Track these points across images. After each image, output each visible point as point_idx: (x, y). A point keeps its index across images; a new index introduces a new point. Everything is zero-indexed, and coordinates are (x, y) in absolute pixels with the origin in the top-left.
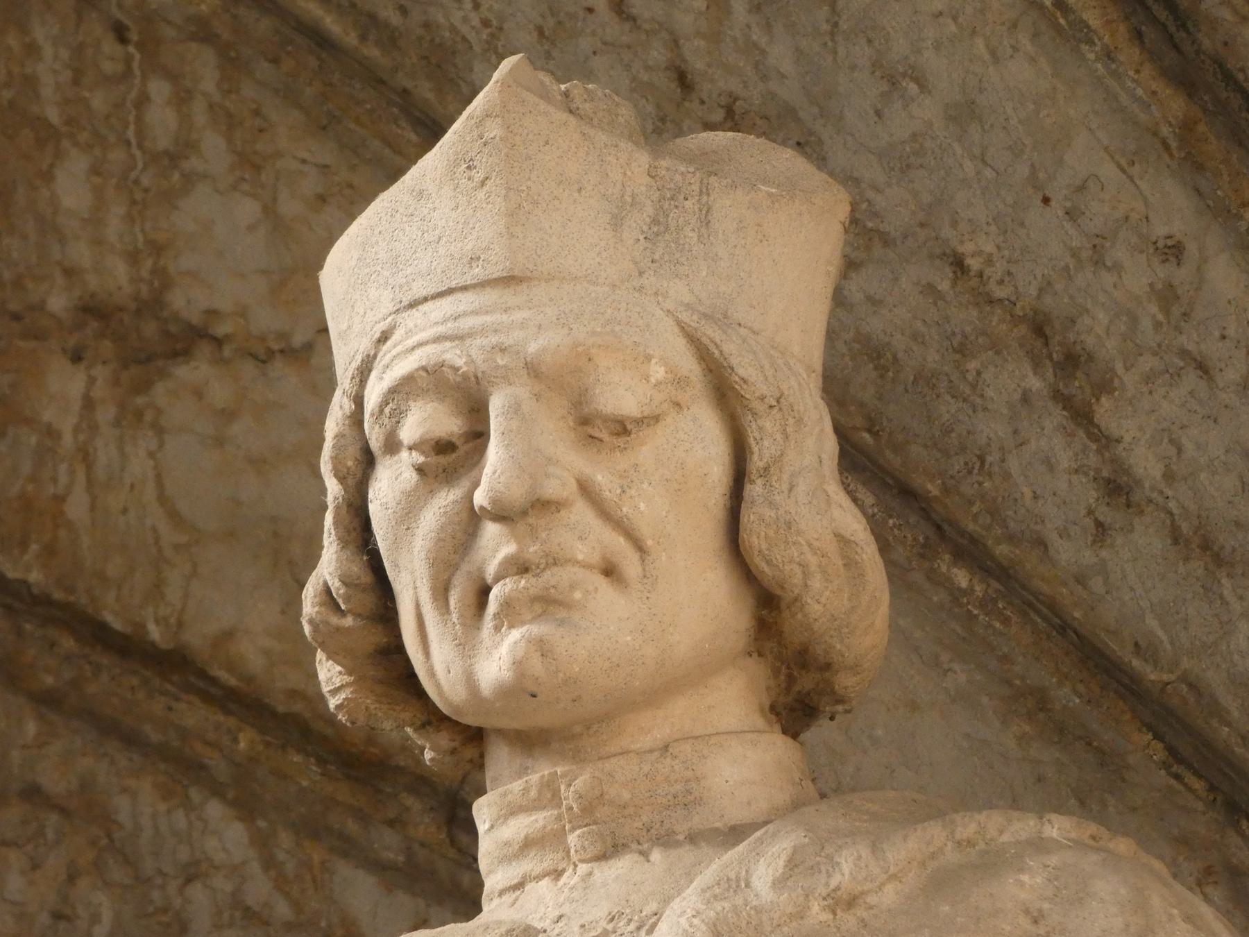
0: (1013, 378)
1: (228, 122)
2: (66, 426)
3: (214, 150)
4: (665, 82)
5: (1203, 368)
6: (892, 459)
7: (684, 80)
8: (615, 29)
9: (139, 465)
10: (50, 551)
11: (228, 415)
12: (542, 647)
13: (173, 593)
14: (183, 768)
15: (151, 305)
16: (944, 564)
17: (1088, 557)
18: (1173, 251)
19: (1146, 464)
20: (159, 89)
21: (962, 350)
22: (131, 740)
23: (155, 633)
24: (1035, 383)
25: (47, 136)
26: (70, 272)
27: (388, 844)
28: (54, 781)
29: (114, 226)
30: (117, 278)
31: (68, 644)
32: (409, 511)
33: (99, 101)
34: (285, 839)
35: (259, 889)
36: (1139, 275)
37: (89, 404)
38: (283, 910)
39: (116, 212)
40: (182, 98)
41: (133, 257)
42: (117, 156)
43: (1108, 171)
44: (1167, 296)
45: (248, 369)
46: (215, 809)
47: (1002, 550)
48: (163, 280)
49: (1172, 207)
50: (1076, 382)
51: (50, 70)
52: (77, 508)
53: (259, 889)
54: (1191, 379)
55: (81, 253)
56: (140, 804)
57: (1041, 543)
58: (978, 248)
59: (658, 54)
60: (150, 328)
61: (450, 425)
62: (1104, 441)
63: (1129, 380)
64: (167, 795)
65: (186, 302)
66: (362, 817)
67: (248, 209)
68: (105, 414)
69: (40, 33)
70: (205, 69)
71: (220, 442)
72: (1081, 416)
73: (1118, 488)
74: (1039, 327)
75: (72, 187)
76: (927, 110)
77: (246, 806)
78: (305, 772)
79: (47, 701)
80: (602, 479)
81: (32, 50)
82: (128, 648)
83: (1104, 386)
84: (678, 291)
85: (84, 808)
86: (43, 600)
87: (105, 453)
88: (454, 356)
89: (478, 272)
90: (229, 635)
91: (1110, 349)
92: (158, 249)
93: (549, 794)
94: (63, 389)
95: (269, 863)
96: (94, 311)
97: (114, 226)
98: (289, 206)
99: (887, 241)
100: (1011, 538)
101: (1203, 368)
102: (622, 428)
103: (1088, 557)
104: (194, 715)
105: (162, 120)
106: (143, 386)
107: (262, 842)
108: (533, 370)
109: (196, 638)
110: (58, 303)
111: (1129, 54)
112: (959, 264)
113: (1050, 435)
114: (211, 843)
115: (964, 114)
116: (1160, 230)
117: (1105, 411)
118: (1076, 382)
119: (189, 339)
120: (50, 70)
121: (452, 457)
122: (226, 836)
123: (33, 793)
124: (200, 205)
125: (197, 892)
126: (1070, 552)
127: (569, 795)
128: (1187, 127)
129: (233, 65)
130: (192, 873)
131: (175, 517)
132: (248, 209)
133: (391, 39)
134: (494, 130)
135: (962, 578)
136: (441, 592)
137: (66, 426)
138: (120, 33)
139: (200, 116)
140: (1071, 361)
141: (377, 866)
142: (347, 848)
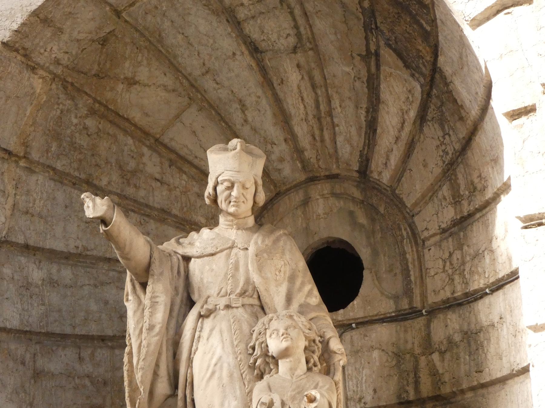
0: (236, 106)
1: (147, 60)
2: (120, 91)
3: (145, 62)
4: (202, 64)
5: (259, 111)
6: (219, 111)
7: (204, 64)
8: (197, 57)
9: (127, 96)
10: (115, 105)
11: (140, 92)
12: (237, 211)
13: (128, 112)
14: (126, 132)
15: (133, 78)
16: (222, 122)
17: (240, 128)
18: (259, 97)
19: (250, 119)
20: (140, 55)
21: (230, 101)
22: (120, 128)
23: (125, 116)
24: (238, 107)
25: (126, 59)
26: (124, 74)
27: (148, 143)
28: (111, 132)
29: (131, 69)
30: (130, 75)
31: (114, 114)
32: (223, 192)
33: (133, 55)
34: (137, 142)
35: (133, 148)
36: (254, 99)
37: (123, 89)
38: (135, 151)
39: (131, 67)
40: (143, 56)
41: (132, 73)
42: (133, 61)
43: (253, 86)
44: (257, 102)
45: (143, 87)
46: (129, 138)
47: (230, 124)
48: (135, 76)
49: (260, 92)
50: (243, 107)
51: (128, 52)
52: (119, 101)
53: (133, 148)
54: (258, 111)
55: (126, 72)
56: (121, 136)
57: (235, 125)
58: (235, 90)
59: (202, 61)
60: (132, 81)
61: (230, 185)
62: (245, 115)
63: (250, 110)
64: (124, 135)
65: (137, 79)
66: (145, 139)
67: (147, 69)
68: (125, 90)
69: (128, 47)
70: (146, 51)
71: (138, 95)
72: (243, 112)
73: (246, 121)
74: (240, 101)
75: (127, 64)
76: (233, 74)
77: (133, 137)
78: (139, 133)
79: (111, 122)
80: (245, 193)
81: (127, 49)
82: (122, 117)
83: (246, 109)
84: (253, 173)
85: (115, 136)
86: (113, 111)
87: (123, 95)
88: (232, 178)
89: (235, 170)
90: (134, 117)
91: (249, 106)
92: (135, 72)
93: (232, 221)
94: (120, 87)
95: (135, 145)
96: (126, 78)
97: (131, 69)
98: (152, 70)
99: (224, 87)
100: (232, 123)
101: (259, 111)
102: (247, 188)
103: (240, 128)
104: (127, 124)
105: (140, 58)
106: (129, 87)
107: (134, 142)
108: (240, 182)
109: (130, 117)
110: (122, 77)
111: (258, 73)
112: (232, 91)
113: (239, 113)
114: (128, 142)
115: (237, 76)
116: (258, 94)
117: (246, 112)
118: (243, 107)
119: (136, 83)
120: (128, 52)
121: (231, 188)
122: (130, 141)
123: (108, 134)
124: (142, 68)
125: (126, 147)
126: (238, 127)
127: (235, 222)
128: (263, 83)
129: (149, 52)
130: (126, 145)
131: (130, 102)
132: (147, 69)
133: (169, 53)
134: (238, 154)
135: (223, 124)
136: (225, 200)
137: (120, 91)
138: (137, 48)
139: (144, 58)
140: (244, 105)
141: (147, 146)
142: (144, 144)
